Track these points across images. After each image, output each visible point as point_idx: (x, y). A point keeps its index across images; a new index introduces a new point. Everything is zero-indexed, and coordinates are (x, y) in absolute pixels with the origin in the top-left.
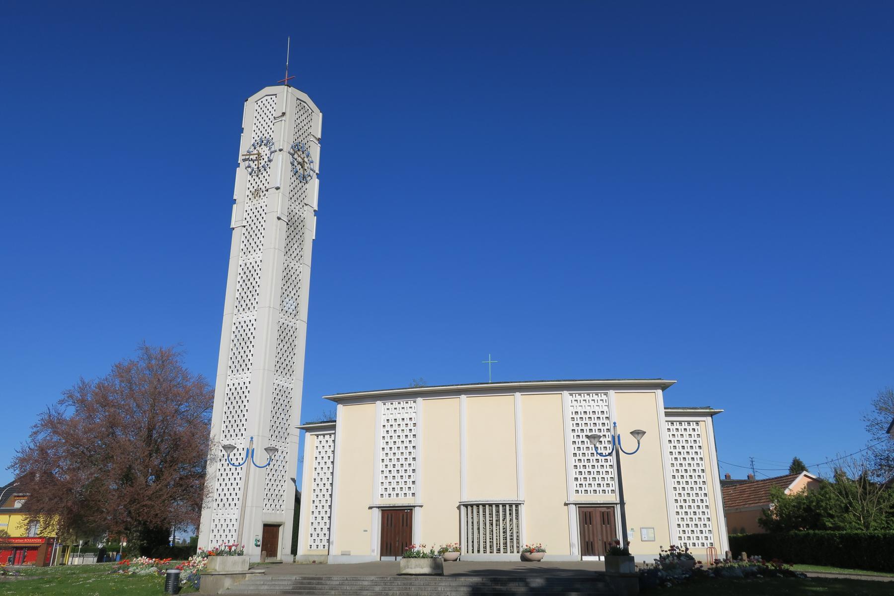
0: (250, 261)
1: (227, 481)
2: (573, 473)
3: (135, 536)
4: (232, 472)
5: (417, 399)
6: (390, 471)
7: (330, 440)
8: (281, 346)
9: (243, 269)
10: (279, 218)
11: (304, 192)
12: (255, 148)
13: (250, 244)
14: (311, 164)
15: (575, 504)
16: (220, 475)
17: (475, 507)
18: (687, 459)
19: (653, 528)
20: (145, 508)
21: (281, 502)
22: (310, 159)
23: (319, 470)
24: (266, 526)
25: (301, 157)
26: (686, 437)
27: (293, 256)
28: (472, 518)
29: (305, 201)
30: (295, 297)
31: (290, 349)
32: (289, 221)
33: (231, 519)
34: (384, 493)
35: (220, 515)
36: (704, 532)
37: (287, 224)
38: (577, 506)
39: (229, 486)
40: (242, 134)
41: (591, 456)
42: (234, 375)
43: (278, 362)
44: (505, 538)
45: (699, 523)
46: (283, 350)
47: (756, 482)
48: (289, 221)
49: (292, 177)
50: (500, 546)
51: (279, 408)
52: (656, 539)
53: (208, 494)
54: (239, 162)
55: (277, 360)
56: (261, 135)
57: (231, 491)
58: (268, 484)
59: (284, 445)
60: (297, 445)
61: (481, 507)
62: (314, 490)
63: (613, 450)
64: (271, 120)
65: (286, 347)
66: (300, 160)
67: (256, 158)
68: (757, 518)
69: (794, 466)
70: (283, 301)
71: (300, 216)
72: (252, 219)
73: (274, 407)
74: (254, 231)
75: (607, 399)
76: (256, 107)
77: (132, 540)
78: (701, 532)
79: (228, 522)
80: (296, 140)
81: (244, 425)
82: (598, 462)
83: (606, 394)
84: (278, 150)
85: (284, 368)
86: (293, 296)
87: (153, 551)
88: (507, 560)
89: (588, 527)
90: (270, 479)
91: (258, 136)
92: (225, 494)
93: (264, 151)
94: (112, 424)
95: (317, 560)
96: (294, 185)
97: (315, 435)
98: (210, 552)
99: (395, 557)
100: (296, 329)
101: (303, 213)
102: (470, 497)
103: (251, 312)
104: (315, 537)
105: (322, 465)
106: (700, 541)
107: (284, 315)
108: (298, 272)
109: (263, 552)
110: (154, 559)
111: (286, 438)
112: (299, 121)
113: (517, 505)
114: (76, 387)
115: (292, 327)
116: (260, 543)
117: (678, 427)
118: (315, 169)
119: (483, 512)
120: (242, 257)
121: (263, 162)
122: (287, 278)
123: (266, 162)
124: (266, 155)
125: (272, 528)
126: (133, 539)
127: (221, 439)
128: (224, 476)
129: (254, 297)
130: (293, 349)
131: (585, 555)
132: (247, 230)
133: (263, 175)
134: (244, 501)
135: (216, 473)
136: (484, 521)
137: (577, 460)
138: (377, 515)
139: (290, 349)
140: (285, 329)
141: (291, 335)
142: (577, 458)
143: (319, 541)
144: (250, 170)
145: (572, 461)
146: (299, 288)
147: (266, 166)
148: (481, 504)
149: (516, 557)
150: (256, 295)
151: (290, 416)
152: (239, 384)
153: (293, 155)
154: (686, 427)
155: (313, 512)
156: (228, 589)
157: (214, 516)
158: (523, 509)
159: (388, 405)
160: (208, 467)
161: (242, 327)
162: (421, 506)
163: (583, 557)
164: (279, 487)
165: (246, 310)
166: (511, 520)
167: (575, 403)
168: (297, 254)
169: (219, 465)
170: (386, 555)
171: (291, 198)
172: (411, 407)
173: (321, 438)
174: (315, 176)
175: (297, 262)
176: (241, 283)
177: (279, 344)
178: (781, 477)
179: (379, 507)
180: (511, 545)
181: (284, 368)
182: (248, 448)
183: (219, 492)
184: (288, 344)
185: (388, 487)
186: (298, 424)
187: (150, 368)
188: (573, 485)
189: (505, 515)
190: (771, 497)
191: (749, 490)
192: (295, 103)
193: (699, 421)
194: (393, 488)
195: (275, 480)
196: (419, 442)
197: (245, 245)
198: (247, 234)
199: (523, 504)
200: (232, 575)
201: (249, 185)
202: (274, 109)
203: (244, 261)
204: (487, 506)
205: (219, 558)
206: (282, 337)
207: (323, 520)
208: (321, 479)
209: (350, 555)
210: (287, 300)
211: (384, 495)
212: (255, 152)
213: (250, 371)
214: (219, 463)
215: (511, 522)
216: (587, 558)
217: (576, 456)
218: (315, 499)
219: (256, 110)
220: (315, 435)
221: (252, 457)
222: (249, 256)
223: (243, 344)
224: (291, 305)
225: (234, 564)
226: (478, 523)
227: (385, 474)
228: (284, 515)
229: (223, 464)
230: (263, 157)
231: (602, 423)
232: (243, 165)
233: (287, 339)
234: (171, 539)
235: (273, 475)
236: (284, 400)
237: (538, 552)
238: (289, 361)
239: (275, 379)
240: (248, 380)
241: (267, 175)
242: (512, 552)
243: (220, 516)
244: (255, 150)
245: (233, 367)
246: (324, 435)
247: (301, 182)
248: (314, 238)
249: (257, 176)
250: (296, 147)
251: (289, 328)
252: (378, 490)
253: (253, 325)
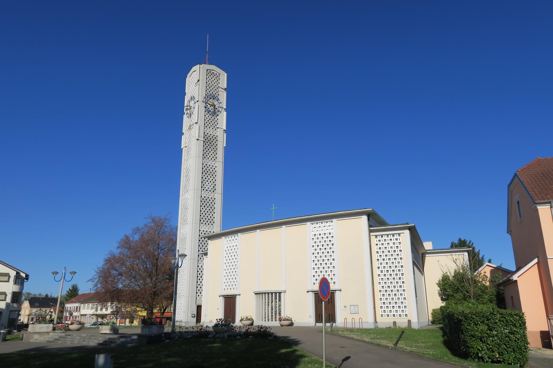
26: (391, 245)
97: (375, 235)
102: (258, 290)
113: (280, 293)
117: (392, 238)
142: (379, 255)
148: (266, 293)
149: (277, 324)
154: (380, 239)
156: (37, 339)
162: (240, 295)
179: (312, 291)
193: (400, 233)
200: (39, 333)
225: (41, 328)
242: (276, 321)
246: (388, 235)
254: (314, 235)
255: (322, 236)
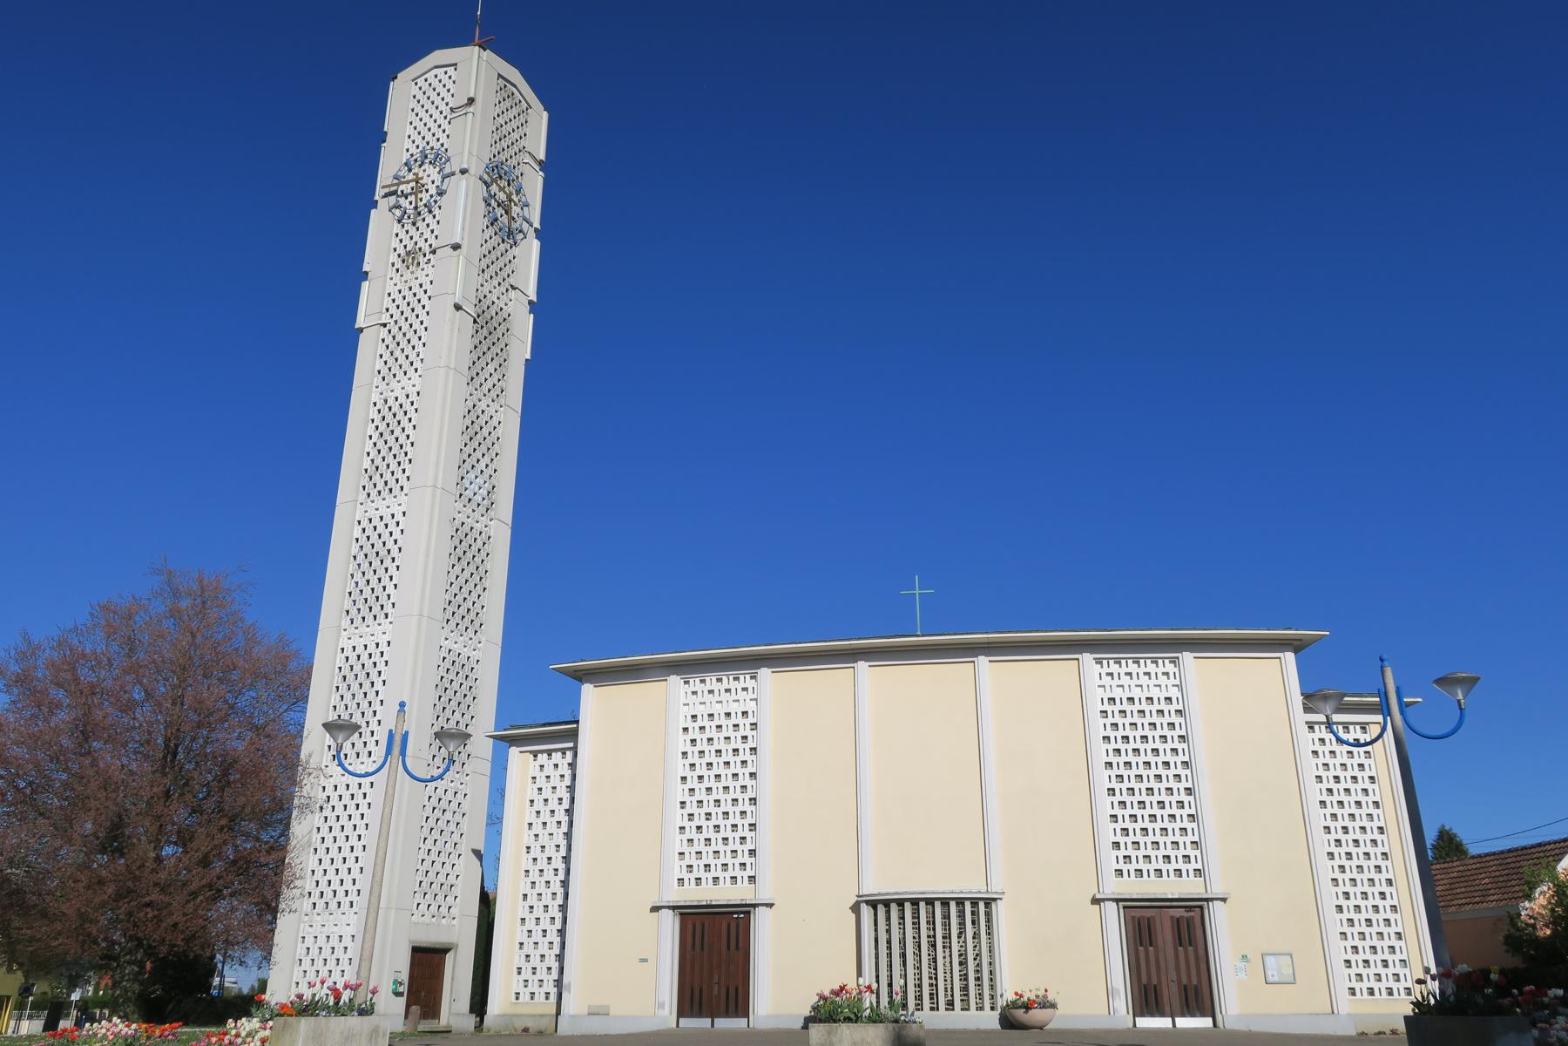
0: (396, 394)
1: (334, 853)
2: (1108, 833)
3: (129, 974)
4: (345, 833)
5: (759, 671)
6: (699, 828)
7: (564, 762)
8: (458, 569)
9: (379, 411)
10: (458, 307)
11: (510, 262)
12: (410, 170)
13: (396, 360)
14: (525, 208)
15: (1117, 901)
16: (319, 840)
17: (894, 907)
18: (1328, 804)
19: (1291, 955)
20: (149, 910)
21: (450, 899)
22: (523, 199)
23: (538, 828)
24: (417, 951)
25: (505, 193)
27: (485, 388)
28: (889, 931)
29: (512, 280)
30: (488, 472)
31: (476, 577)
32: (479, 316)
33: (341, 937)
34: (685, 876)
35: (317, 927)
36: (1391, 963)
37: (475, 321)
38: (1121, 904)
39: (338, 863)
40: (384, 145)
41: (1148, 795)
42: (356, 628)
43: (450, 602)
44: (965, 977)
45: (1378, 944)
46: (462, 580)
47: (1521, 850)
48: (479, 316)
49: (485, 228)
50: (952, 996)
51: (450, 700)
52: (1297, 978)
53: (292, 881)
54: (377, 198)
55: (448, 597)
56: (422, 144)
57: (343, 874)
58: (423, 860)
59: (459, 779)
60: (486, 781)
61: (908, 907)
62: (527, 871)
63: (1384, 729)
64: (444, 114)
65: (467, 574)
66: (502, 196)
67: (412, 189)
68: (1502, 934)
69: (1440, 842)
70: (462, 478)
71: (501, 309)
72: (400, 309)
73: (440, 697)
74: (404, 334)
75: (1176, 670)
76: (415, 90)
77: (120, 982)
78: (1385, 963)
79: (334, 942)
80: (494, 156)
81: (354, 904)
82: (1164, 808)
83: (1174, 661)
84: (457, 172)
85: (463, 617)
86: (484, 469)
87: (170, 1007)
88: (971, 1026)
89: (1147, 951)
90: (429, 850)
91: (418, 147)
92: (330, 881)
93: (429, 176)
94: (85, 731)
95: (530, 1024)
96: (489, 246)
97: (530, 752)
98: (283, 1006)
99: (710, 1019)
100: (489, 538)
101: (506, 305)
102: (875, 886)
103: (395, 497)
104: (527, 974)
105: (545, 816)
106: (1384, 985)
107: (465, 506)
108: (494, 422)
109: (414, 1008)
110: (134, 1026)
111: (463, 764)
112: (501, 120)
113: (989, 902)
114: (13, 653)
115: (481, 533)
116: (404, 989)
118: (531, 220)
119: (913, 918)
120: (377, 387)
121: (425, 197)
122: (471, 432)
123: (431, 196)
124: (433, 182)
125: (430, 955)
126: (123, 981)
127: (324, 764)
128: (329, 842)
129: (402, 467)
130: (481, 578)
131: (1142, 1015)
132: (390, 331)
133: (426, 222)
134: (379, 868)
135: (310, 839)
136: (914, 938)
137: (1116, 804)
138: (669, 925)
139: (476, 577)
140: (467, 535)
141: (479, 550)
143: (537, 983)
144: (398, 213)
145: (1105, 805)
146: (497, 454)
147: (433, 204)
150: (407, 462)
151: (472, 717)
152: (366, 646)
153: (487, 185)
155: (523, 919)
157: (304, 929)
158: (1001, 911)
159: (695, 683)
160: (294, 823)
161: (375, 528)
162: (770, 905)
163: (1137, 1019)
164: (448, 867)
165: (385, 493)
166: (976, 936)
167: (1107, 680)
168: (494, 385)
169: (317, 819)
170: (691, 1015)
171: (483, 271)
172: (745, 689)
173: (543, 758)
174: (531, 234)
175: (493, 401)
176: (374, 440)
177: (454, 566)
178: (1525, 848)
180: (977, 992)
181: (463, 617)
182: (391, 731)
183: (316, 878)
184: (472, 568)
185: (694, 863)
186: (491, 730)
187: (174, 613)
188: (1110, 859)
189: (962, 924)
190: (1526, 887)
191: (1443, 876)
192: (495, 84)
193: (1368, 723)
194: (706, 866)
195: (440, 852)
196: (766, 764)
197: (386, 363)
198: (389, 340)
199: (1001, 899)
201: (395, 243)
202: (451, 92)
203: (381, 394)
204: (922, 904)
205: (305, 1024)
206: (459, 552)
207: (545, 936)
208: (543, 847)
209: (608, 1014)
210: (472, 476)
211: (686, 882)
212: (411, 176)
213: (389, 619)
214: (317, 815)
215: (977, 941)
216: (1146, 1023)
217: (1114, 795)
218: (528, 891)
219: (414, 97)
220: (530, 752)
221: (403, 753)
222: (394, 384)
223: (376, 563)
224: (480, 488)
226: (903, 942)
227: (688, 835)
228: (457, 927)
229: (326, 818)
230: (426, 187)
231: (1169, 724)
232: (384, 204)
233: (469, 555)
234: (216, 981)
235: (436, 841)
236: (461, 684)
237: (1044, 1007)
238: (474, 603)
239: (443, 639)
240: (386, 638)
241: (435, 221)
242: (980, 1008)
243: (316, 930)
244: (411, 174)
245: (354, 612)
246: (549, 753)
247: (503, 241)
248: (528, 357)
249: (414, 224)
250: (496, 171)
251: (475, 534)
252: (673, 868)
253: (391, 580)
254: (689, 718)
255: (733, 721)
